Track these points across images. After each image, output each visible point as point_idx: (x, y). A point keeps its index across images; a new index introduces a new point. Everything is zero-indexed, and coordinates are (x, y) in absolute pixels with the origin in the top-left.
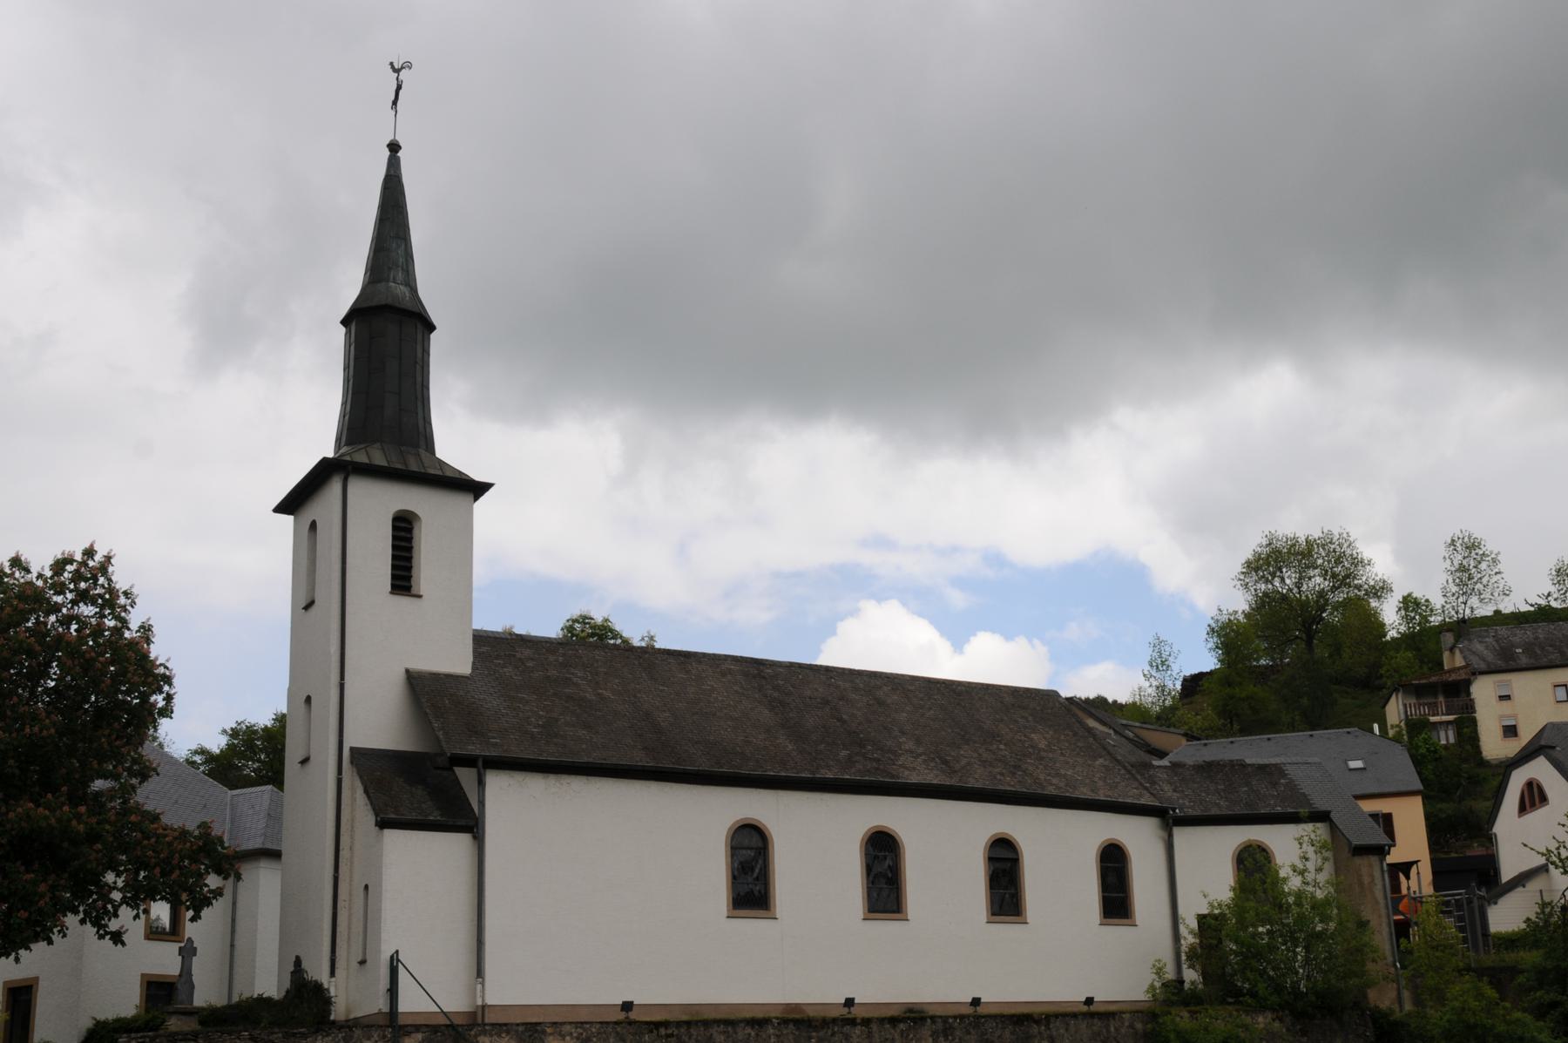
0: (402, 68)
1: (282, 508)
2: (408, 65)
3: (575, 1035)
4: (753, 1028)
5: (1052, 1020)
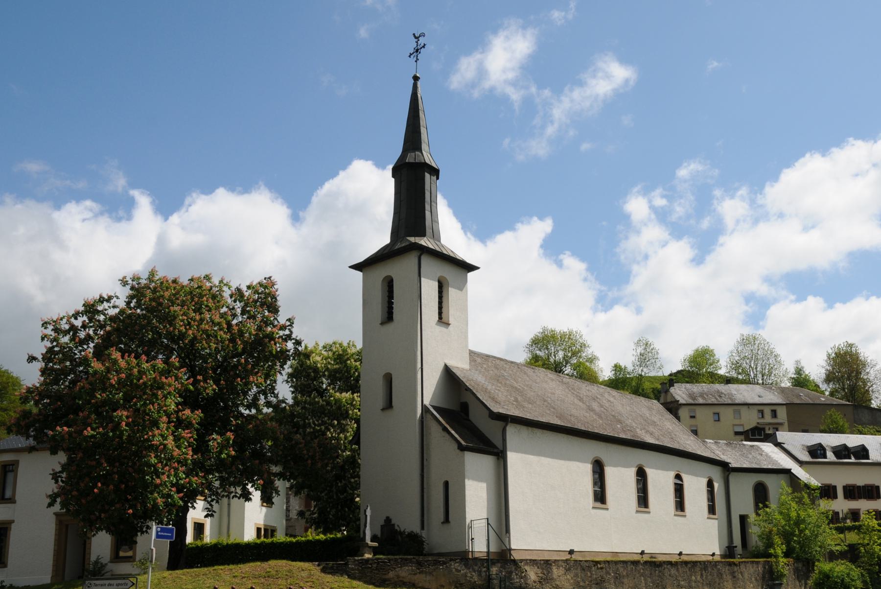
0: (420, 36)
1: (358, 267)
2: (423, 35)
3: (564, 566)
4: (634, 565)
5: (741, 563)
